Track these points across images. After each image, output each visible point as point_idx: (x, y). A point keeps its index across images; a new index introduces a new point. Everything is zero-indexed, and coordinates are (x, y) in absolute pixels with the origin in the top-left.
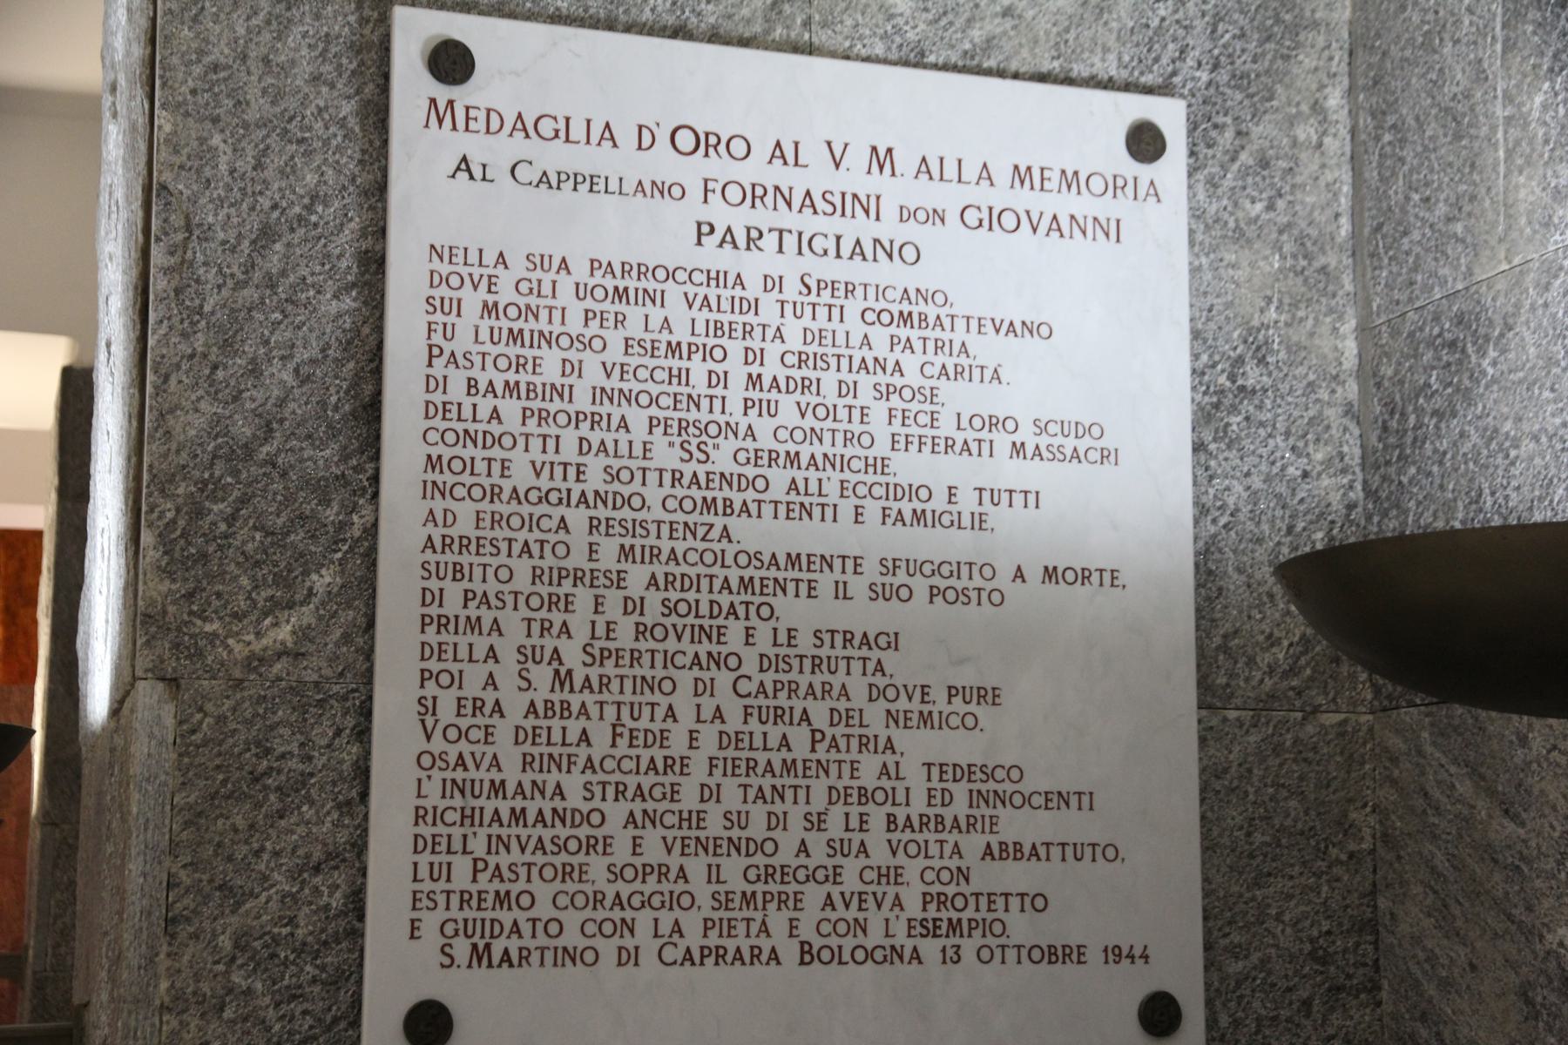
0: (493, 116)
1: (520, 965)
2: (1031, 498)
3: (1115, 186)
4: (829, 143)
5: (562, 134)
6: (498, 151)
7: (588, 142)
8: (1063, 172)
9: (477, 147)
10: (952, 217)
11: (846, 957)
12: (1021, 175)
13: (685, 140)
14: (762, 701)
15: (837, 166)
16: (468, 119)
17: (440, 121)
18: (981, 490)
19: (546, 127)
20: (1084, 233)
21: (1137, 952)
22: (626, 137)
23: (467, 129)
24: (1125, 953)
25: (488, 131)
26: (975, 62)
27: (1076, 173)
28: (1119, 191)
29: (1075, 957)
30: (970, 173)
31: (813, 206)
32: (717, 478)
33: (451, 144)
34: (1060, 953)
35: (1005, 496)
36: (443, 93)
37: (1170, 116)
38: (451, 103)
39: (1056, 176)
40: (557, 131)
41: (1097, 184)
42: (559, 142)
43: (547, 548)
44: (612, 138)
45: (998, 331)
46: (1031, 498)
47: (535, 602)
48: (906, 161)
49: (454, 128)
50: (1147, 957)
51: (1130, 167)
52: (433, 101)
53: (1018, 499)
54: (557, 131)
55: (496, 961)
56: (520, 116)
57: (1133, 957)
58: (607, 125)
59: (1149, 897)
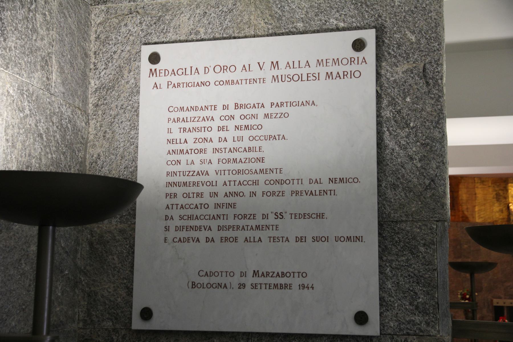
3: (351, 61)
4: (259, 63)
5: (184, 73)
8: (334, 59)
11: (205, 286)
13: (218, 69)
15: (261, 69)
21: (310, 286)
22: (201, 70)
26: (168, 39)
28: (352, 63)
32: (322, 192)
34: (284, 286)
36: (153, 67)
38: (155, 70)
41: (345, 61)
42: (183, 75)
50: (313, 288)
51: (355, 54)
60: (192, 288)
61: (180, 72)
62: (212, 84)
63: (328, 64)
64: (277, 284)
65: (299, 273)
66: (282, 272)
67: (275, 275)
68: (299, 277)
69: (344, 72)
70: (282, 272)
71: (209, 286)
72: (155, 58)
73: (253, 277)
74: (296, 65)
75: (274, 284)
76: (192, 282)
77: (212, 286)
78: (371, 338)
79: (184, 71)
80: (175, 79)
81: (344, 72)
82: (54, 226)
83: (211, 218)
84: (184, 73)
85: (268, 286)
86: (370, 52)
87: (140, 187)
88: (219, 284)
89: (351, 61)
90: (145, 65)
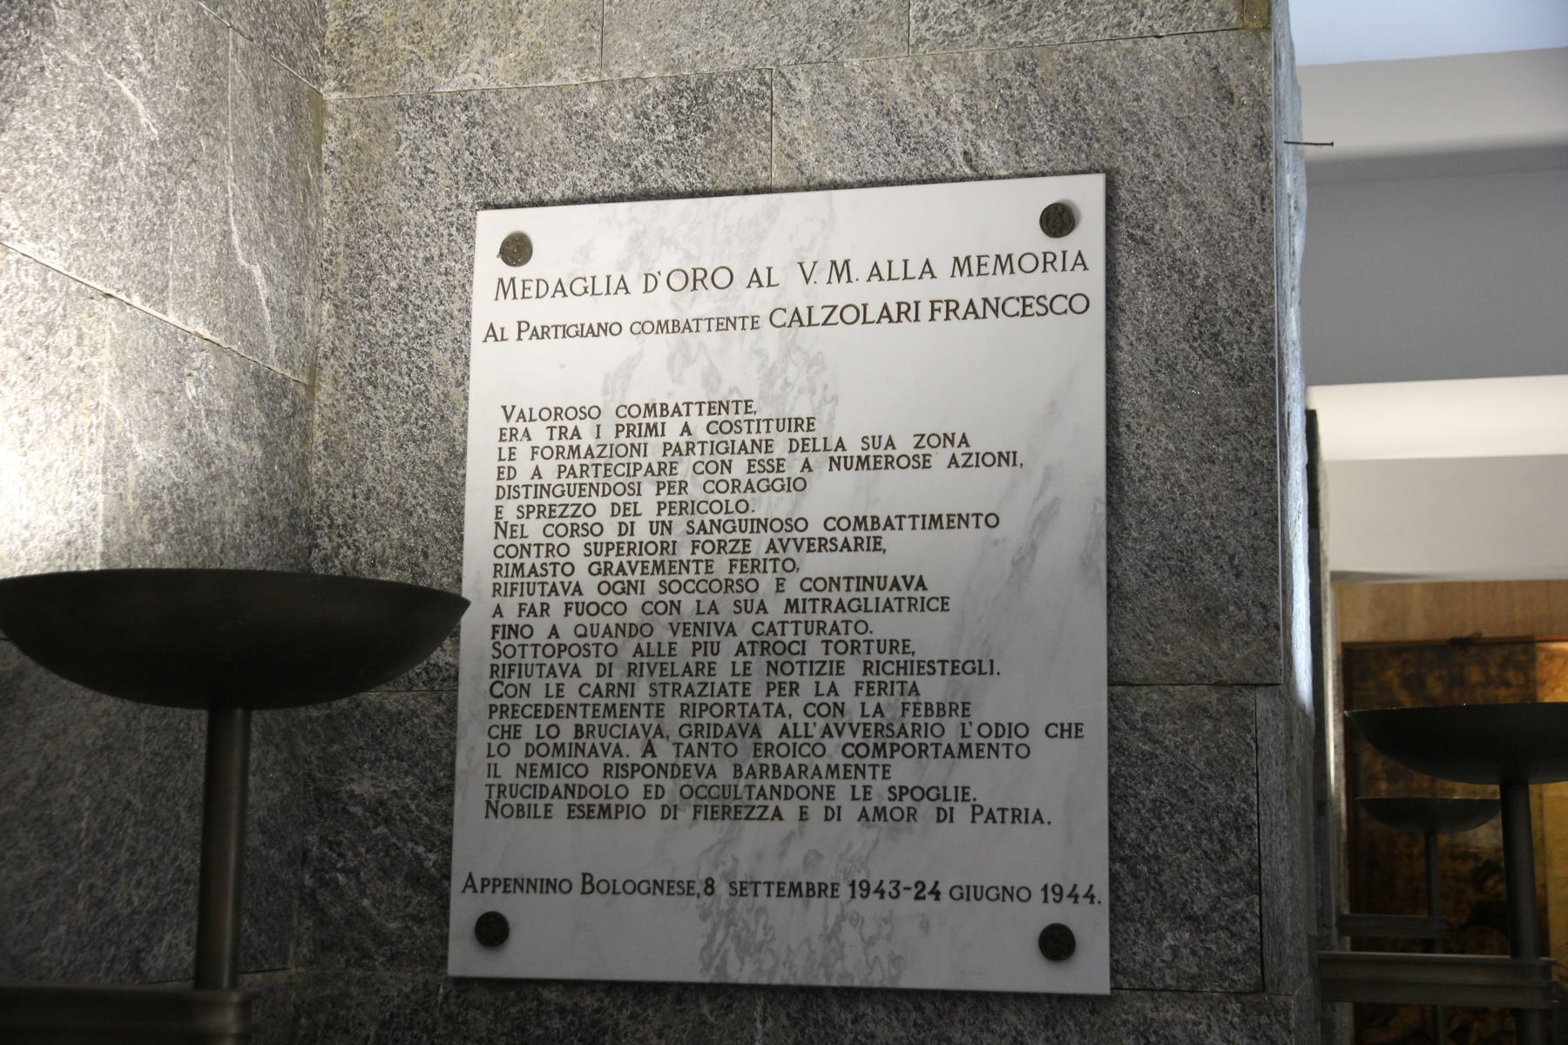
3: (1046, 262)
11: (619, 888)
12: (961, 265)
14: (597, 699)
15: (807, 281)
17: (505, 294)
21: (1081, 891)
27: (1009, 256)
28: (699, 284)
30: (915, 270)
36: (508, 272)
38: (513, 280)
39: (991, 261)
43: (851, 626)
47: (549, 651)
48: (860, 269)
50: (1092, 897)
58: (1080, 254)
60: (584, 892)
61: (578, 287)
63: (527, 293)
64: (799, 884)
71: (629, 887)
72: (516, 250)
76: (584, 875)
77: (637, 888)
79: (589, 283)
82: (248, 708)
85: (774, 889)
86: (1089, 235)
87: (465, 604)
88: (1004, 888)
90: (488, 265)
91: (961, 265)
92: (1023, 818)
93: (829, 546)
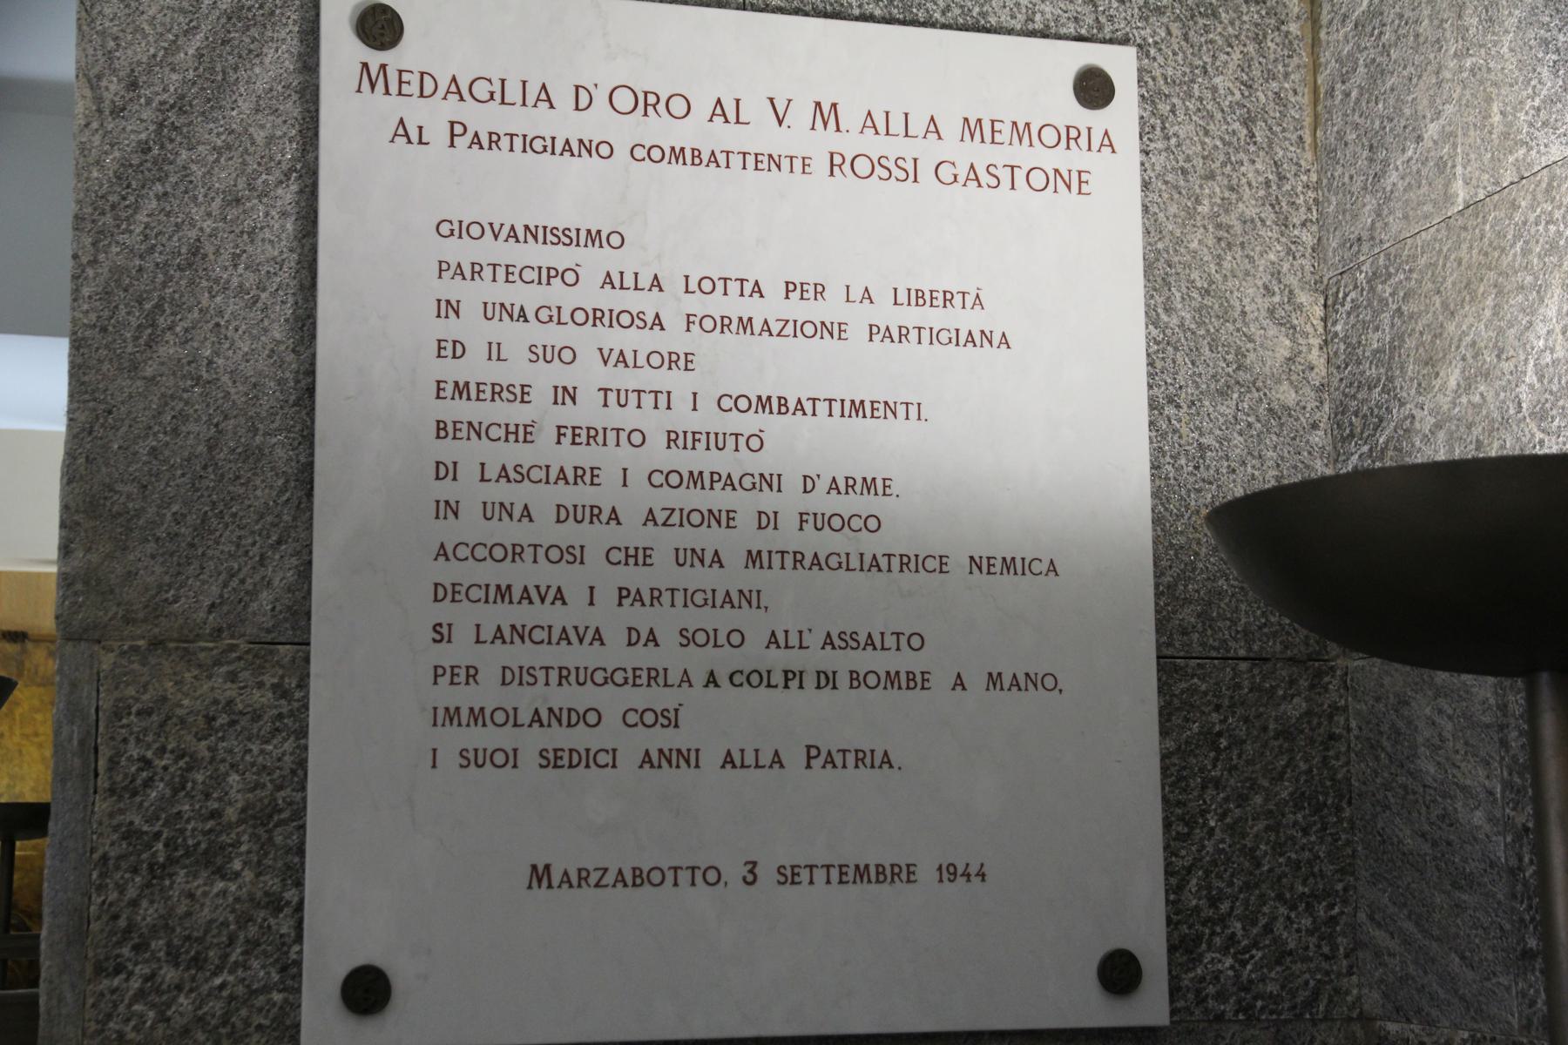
0: (427, 78)
1: (579, 886)
2: (662, 399)
3: (1069, 137)
4: (771, 100)
6: (434, 115)
7: (524, 104)
8: (1015, 123)
9: (417, 112)
10: (926, 171)
12: (972, 128)
13: (624, 100)
16: (401, 82)
17: (373, 86)
18: (606, 390)
19: (481, 90)
20: (1069, 187)
21: (973, 870)
22: (563, 98)
23: (400, 94)
24: (960, 871)
25: (422, 95)
27: (1028, 124)
28: (1072, 142)
29: (904, 876)
30: (918, 127)
31: (977, 179)
33: (387, 108)
34: (888, 872)
35: (633, 397)
36: (375, 58)
37: (1120, 64)
38: (383, 67)
40: (492, 94)
41: (1049, 136)
44: (549, 100)
45: (496, 237)
46: (662, 399)
49: (387, 92)
50: (983, 875)
52: (365, 65)
53: (648, 400)
54: (492, 94)
55: (555, 882)
56: (454, 79)
57: (969, 875)
59: (1078, 837)
61: (481, 90)
62: (622, 153)
64: (867, 866)
65: (693, 869)
66: (634, 869)
67: (610, 878)
68: (693, 884)
69: (452, 123)
70: (634, 869)
73: (530, 887)
74: (897, 125)
75: (857, 867)
78: (1150, 1032)
80: (482, 118)
81: (452, 123)
83: (555, 639)
84: (498, 96)
89: (646, 105)
91: (972, 128)
92: (868, 761)
93: (505, 394)
